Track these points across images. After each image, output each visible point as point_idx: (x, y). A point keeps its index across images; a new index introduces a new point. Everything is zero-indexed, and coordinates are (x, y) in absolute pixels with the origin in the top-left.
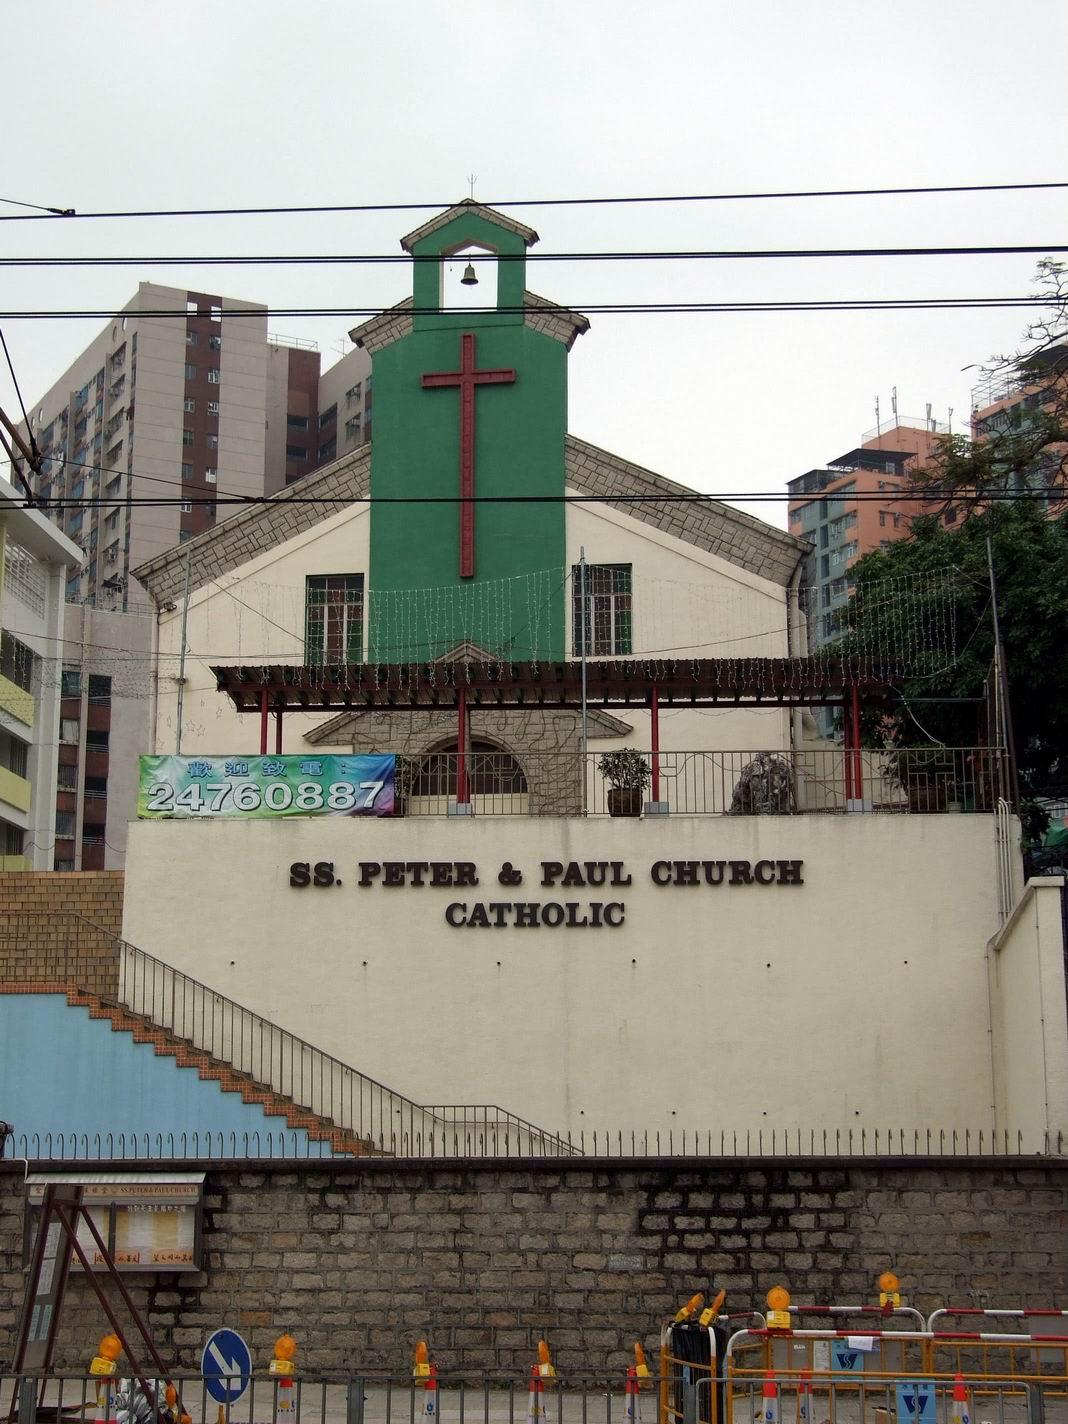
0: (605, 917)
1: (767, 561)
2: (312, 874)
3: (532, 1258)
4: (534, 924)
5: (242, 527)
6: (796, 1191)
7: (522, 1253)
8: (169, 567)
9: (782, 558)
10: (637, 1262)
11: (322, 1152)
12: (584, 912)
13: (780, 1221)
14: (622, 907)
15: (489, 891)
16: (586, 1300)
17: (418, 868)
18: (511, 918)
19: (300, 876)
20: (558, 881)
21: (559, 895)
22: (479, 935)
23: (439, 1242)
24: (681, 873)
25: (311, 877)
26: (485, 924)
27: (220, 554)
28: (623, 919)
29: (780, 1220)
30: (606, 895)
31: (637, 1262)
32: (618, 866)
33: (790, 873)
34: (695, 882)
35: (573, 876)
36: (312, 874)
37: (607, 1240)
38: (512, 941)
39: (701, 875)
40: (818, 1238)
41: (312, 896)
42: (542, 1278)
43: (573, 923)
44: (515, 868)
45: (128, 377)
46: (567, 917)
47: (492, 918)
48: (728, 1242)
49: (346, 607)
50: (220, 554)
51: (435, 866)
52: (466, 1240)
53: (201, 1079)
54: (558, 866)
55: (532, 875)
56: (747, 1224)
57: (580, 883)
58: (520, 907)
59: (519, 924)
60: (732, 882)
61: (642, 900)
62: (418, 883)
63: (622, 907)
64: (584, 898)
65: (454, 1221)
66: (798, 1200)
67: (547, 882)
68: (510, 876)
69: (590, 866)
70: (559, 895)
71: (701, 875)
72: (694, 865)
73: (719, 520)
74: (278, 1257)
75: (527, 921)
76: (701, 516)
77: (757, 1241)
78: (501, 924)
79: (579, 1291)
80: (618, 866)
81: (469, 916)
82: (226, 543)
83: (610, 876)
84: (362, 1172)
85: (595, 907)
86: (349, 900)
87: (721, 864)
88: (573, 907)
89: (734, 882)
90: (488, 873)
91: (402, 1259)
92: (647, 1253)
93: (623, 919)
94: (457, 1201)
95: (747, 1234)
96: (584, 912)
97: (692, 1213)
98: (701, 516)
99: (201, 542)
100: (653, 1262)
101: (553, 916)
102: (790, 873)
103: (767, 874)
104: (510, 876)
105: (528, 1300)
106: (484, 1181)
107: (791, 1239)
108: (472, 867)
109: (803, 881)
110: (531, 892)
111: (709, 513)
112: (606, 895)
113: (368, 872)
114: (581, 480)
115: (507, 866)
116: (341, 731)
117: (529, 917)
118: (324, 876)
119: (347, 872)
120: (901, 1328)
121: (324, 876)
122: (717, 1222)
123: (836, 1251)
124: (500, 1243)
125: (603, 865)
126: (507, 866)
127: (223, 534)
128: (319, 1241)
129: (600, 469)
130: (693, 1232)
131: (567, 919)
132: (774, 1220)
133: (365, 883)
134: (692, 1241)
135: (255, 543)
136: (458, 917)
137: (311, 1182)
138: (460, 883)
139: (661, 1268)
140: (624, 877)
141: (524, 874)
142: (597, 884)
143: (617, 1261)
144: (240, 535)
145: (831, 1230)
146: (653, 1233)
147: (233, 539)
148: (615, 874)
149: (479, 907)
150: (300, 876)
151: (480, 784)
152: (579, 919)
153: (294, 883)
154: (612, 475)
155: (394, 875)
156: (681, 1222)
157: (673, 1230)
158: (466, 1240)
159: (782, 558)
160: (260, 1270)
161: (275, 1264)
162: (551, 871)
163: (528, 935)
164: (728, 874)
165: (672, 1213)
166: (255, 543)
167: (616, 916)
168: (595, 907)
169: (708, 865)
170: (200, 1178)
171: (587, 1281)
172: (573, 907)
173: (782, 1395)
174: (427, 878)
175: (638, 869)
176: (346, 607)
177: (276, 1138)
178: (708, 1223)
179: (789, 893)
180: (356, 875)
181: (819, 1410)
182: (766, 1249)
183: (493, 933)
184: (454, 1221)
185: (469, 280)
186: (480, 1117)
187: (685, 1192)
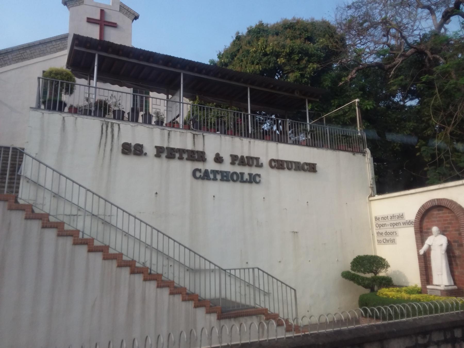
2: (133, 149)
4: (227, 180)
5: (20, 50)
12: (246, 177)
15: (211, 165)
18: (219, 177)
20: (237, 162)
21: (238, 169)
32: (257, 159)
33: (312, 168)
36: (133, 149)
43: (243, 181)
47: (212, 176)
55: (227, 159)
59: (222, 180)
62: (181, 158)
63: (259, 176)
64: (246, 170)
67: (233, 163)
70: (238, 169)
81: (202, 174)
82: (12, 55)
83: (255, 163)
85: (250, 175)
87: (291, 162)
90: (210, 156)
93: (260, 180)
96: (246, 177)
102: (312, 168)
110: (227, 167)
112: (255, 171)
113: (160, 151)
115: (217, 155)
126: (217, 155)
131: (240, 179)
133: (158, 155)
135: (24, 56)
136: (198, 174)
140: (260, 164)
152: (245, 179)
162: (234, 158)
167: (258, 179)
168: (250, 175)
172: (242, 174)
180: (154, 152)
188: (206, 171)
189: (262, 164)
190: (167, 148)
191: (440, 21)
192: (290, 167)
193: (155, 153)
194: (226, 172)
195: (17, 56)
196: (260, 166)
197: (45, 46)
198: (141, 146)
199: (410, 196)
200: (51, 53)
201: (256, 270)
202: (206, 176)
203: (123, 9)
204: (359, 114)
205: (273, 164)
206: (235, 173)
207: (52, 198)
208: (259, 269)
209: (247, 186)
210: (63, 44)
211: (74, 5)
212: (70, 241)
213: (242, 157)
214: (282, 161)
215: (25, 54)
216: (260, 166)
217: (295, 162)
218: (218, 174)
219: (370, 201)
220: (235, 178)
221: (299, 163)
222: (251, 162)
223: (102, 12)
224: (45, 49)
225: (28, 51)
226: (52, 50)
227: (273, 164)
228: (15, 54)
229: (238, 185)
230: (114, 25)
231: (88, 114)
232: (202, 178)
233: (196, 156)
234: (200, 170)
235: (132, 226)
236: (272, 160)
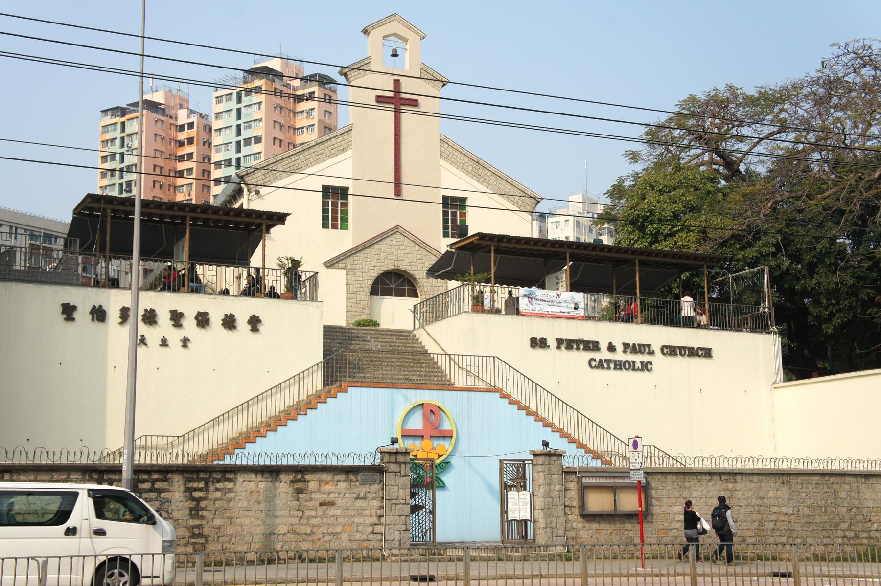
1: (524, 204)
3: (756, 508)
4: (620, 369)
5: (291, 157)
8: (255, 172)
9: (529, 203)
11: (597, 464)
12: (638, 365)
15: (604, 354)
16: (775, 525)
18: (612, 366)
20: (629, 350)
21: (630, 357)
22: (600, 372)
25: (538, 343)
26: (603, 367)
28: (652, 368)
32: (649, 346)
33: (707, 353)
34: (676, 355)
36: (538, 343)
38: (612, 374)
41: (539, 352)
42: (759, 516)
43: (634, 369)
44: (613, 345)
46: (631, 366)
47: (606, 365)
49: (339, 203)
53: (552, 432)
55: (620, 348)
58: (615, 361)
59: (615, 368)
60: (688, 356)
61: (658, 360)
62: (578, 349)
63: (651, 363)
64: (638, 358)
67: (625, 351)
70: (630, 357)
74: (669, 508)
76: (496, 180)
78: (609, 368)
79: (772, 521)
80: (649, 346)
81: (597, 363)
82: (283, 164)
85: (642, 362)
86: (552, 354)
87: (684, 348)
90: (604, 346)
93: (652, 368)
94: (730, 486)
96: (638, 365)
98: (496, 180)
99: (272, 162)
101: (627, 366)
102: (707, 353)
103: (700, 353)
104: (611, 348)
105: (755, 525)
106: (739, 478)
108: (597, 343)
109: (600, 349)
110: (619, 356)
111: (500, 179)
112: (646, 358)
113: (560, 342)
114: (446, 156)
115: (610, 344)
116: (340, 262)
117: (620, 365)
119: (552, 342)
124: (745, 502)
126: (610, 344)
127: (282, 159)
131: (632, 368)
133: (558, 347)
135: (297, 166)
136: (593, 364)
137: (202, 475)
138: (593, 350)
140: (651, 351)
141: (617, 350)
142: (642, 353)
144: (290, 161)
147: (287, 162)
149: (600, 360)
152: (637, 368)
154: (459, 155)
155: (569, 344)
159: (529, 203)
162: (626, 346)
163: (618, 373)
164: (687, 352)
166: (297, 166)
167: (649, 367)
168: (642, 362)
169: (680, 348)
172: (634, 362)
173: (851, 561)
175: (656, 348)
176: (339, 203)
179: (704, 361)
180: (555, 344)
181: (492, 582)
186: (165, 442)
187: (154, 482)
188: (600, 360)
189: (654, 351)
190: (566, 340)
191: (599, 523)
192: (683, 353)
193: (556, 346)
194: (618, 361)
195: (289, 166)
196: (651, 353)
197: (322, 146)
198: (545, 339)
199: (837, 382)
200: (330, 156)
201: (653, 447)
202: (601, 365)
203: (426, 73)
205: (665, 351)
206: (628, 361)
208: (655, 447)
210: (346, 141)
211: (358, 76)
214: (674, 347)
215: (299, 161)
216: (651, 353)
217: (688, 348)
218: (581, 343)
220: (627, 366)
221: (693, 348)
222: (642, 350)
223: (397, 83)
224: (323, 151)
225: (301, 156)
226: (333, 152)
227: (665, 351)
228: (287, 162)
229: (631, 373)
230: (413, 103)
232: (596, 367)
233: (591, 345)
234: (595, 360)
236: (663, 347)
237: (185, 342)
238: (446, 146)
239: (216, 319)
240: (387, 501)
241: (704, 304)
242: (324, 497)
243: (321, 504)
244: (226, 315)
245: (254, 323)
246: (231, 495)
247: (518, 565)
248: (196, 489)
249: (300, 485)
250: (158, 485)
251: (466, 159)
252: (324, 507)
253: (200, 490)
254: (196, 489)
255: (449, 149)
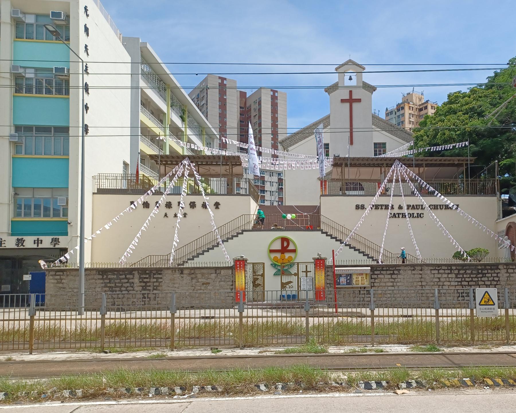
0: (419, 216)
2: (360, 207)
3: (436, 283)
6: (487, 270)
7: (434, 282)
10: (456, 283)
12: (415, 215)
13: (484, 275)
14: (423, 214)
15: (396, 211)
17: (382, 206)
18: (401, 216)
19: (357, 207)
21: (411, 211)
23: (417, 280)
24: (435, 207)
25: (360, 207)
26: (396, 217)
27: (298, 138)
29: (484, 275)
30: (420, 211)
31: (456, 283)
32: (422, 206)
35: (413, 207)
36: (360, 207)
37: (450, 279)
39: (439, 207)
40: (492, 278)
43: (413, 217)
45: (205, 97)
47: (397, 216)
48: (474, 279)
50: (298, 138)
51: (385, 205)
52: (423, 280)
54: (410, 206)
56: (472, 276)
57: (414, 209)
58: (403, 214)
62: (382, 208)
63: (423, 214)
64: (415, 212)
65: (420, 276)
66: (488, 271)
67: (408, 209)
68: (400, 207)
69: (417, 205)
71: (439, 207)
72: (437, 205)
73: (405, 133)
75: (404, 216)
77: (480, 279)
78: (399, 217)
83: (420, 207)
84: (133, 272)
85: (418, 214)
87: (443, 205)
88: (413, 214)
89: (445, 209)
90: (396, 207)
91: (410, 283)
92: (458, 282)
95: (478, 278)
96: (415, 215)
97: (466, 274)
100: (459, 283)
107: (486, 279)
112: (420, 211)
115: (400, 205)
118: (363, 207)
120: (195, 302)
121: (363, 207)
122: (472, 276)
123: (495, 281)
125: (419, 205)
126: (400, 205)
128: (393, 280)
129: (379, 122)
130: (467, 278)
131: (412, 216)
132: (483, 275)
134: (467, 279)
139: (461, 285)
143: (453, 283)
145: (494, 277)
146: (460, 278)
148: (422, 207)
149: (394, 214)
150: (357, 207)
151: (354, 189)
152: (414, 216)
153: (356, 209)
156: (465, 276)
157: (463, 277)
158: (423, 280)
160: (382, 286)
161: (384, 285)
162: (408, 207)
164: (444, 207)
165: (463, 274)
167: (422, 216)
168: (418, 214)
169: (440, 205)
170: (370, 268)
171: (447, 288)
172: (413, 214)
174: (384, 207)
177: (366, 261)
178: (470, 276)
182: (481, 281)
183: (397, 219)
184: (420, 276)
185: (350, 79)
187: (466, 270)
188: (394, 214)
202: (394, 216)
204: (48, 134)
207: (88, 134)
209: (416, 219)
212: (371, 259)
213: (413, 205)
219: (497, 223)
223: (351, 92)
231: (52, 128)
235: (410, 258)
237: (185, 215)
238: (375, 119)
239: (199, 205)
240: (453, 290)
241: (495, 183)
242: (204, 281)
243: (203, 284)
244: (167, 202)
245: (217, 205)
246: (160, 280)
247: (298, 310)
248: (145, 278)
249: (193, 276)
250: (128, 276)
251: (385, 124)
252: (205, 285)
253: (147, 278)
254: (145, 278)
255: (377, 120)
